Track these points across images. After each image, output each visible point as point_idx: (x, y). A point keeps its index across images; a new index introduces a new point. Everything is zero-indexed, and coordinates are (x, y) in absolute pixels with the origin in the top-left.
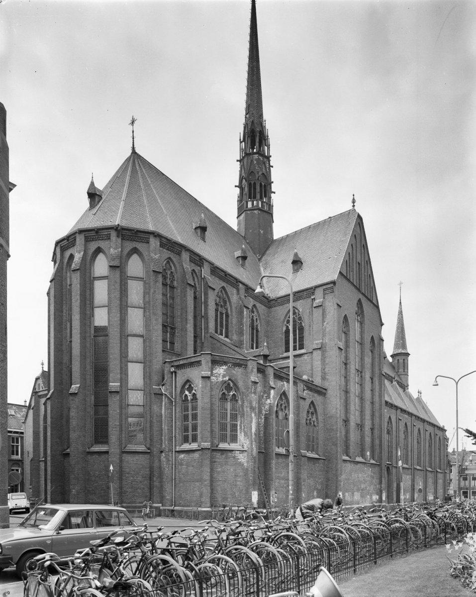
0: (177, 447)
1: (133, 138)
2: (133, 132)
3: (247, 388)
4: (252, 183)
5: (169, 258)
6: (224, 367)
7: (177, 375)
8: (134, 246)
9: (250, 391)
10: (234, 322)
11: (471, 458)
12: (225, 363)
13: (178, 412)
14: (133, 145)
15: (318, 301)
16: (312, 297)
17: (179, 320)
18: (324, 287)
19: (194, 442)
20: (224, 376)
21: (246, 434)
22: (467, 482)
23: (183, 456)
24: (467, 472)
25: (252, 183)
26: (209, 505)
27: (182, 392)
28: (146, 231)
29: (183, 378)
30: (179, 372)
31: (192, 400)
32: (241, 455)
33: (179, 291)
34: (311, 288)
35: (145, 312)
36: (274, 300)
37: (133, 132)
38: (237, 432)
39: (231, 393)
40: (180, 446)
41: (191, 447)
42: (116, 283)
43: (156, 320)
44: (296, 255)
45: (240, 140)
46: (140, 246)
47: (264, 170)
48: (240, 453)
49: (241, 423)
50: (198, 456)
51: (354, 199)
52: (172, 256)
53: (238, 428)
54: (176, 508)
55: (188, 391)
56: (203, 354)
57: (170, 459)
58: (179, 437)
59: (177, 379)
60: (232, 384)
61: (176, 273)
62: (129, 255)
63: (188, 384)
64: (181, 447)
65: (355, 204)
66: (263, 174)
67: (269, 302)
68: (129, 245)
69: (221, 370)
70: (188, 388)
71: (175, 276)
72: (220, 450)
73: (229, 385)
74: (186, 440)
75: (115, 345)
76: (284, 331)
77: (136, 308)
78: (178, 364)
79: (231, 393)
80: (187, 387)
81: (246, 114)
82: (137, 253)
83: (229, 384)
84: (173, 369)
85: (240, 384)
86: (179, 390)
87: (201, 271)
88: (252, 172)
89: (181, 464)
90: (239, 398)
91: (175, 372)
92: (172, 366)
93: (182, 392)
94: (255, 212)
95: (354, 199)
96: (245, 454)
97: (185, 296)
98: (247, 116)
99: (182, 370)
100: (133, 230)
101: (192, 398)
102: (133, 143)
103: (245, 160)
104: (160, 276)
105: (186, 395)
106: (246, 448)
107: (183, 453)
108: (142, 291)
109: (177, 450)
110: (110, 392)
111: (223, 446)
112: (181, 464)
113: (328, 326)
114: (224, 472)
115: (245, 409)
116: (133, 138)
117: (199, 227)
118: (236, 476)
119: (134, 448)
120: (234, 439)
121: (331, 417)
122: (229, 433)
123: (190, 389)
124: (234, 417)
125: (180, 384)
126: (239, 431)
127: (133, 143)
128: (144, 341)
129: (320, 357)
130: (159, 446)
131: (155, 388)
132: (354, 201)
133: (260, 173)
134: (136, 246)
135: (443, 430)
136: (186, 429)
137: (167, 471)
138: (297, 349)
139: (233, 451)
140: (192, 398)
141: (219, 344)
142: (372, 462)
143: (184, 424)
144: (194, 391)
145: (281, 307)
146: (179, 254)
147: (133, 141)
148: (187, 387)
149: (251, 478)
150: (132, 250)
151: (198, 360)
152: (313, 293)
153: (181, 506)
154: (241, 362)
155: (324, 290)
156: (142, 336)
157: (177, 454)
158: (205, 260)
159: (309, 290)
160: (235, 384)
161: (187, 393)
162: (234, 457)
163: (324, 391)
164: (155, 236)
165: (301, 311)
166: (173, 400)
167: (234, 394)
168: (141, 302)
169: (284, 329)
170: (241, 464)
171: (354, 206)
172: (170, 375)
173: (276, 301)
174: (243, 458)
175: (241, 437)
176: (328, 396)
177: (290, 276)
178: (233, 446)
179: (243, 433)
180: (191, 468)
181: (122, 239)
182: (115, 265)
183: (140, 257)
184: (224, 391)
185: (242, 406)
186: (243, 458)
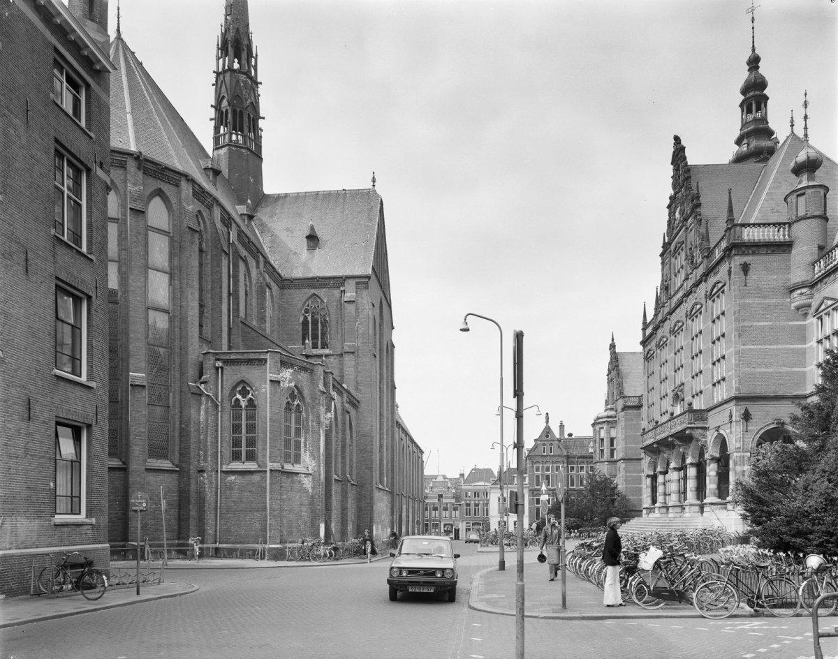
0: (224, 466)
1: (118, 18)
2: (118, 9)
3: (314, 398)
4: (238, 110)
5: (199, 212)
6: (291, 370)
7: (225, 372)
8: (159, 187)
9: (317, 402)
10: (254, 304)
11: (431, 485)
12: (292, 366)
13: (225, 420)
14: (119, 27)
15: (350, 295)
16: (341, 289)
17: (209, 295)
18: (358, 280)
19: (249, 460)
20: (290, 381)
21: (312, 455)
22: (427, 513)
23: (233, 478)
24: (427, 501)
25: (238, 110)
26: (278, 541)
27: (232, 394)
28: (171, 168)
29: (235, 377)
30: (228, 369)
31: (247, 406)
32: (306, 479)
33: (209, 257)
34: (341, 277)
35: (171, 279)
36: (289, 280)
37: (118, 9)
38: (300, 451)
39: (296, 403)
40: (228, 465)
41: (246, 467)
42: (140, 234)
43: (193, 294)
44: (312, 228)
45: (218, 45)
46: (168, 189)
47: (253, 98)
48: (305, 477)
49: (306, 440)
50: (259, 478)
51: (374, 178)
52: (202, 208)
53: (302, 445)
54: (221, 546)
55: (240, 394)
56: (270, 351)
57: (214, 481)
58: (227, 454)
59: (224, 378)
60: (296, 392)
61: (206, 233)
62: (152, 196)
63: (243, 387)
64: (230, 467)
65: (375, 184)
66: (252, 103)
67: (285, 284)
68: (154, 184)
69: (287, 374)
70: (240, 391)
71: (204, 237)
72: (286, 472)
73: (295, 393)
74: (236, 457)
75: (138, 320)
76: (301, 322)
77: (160, 271)
78: (228, 357)
79: (296, 403)
80: (239, 388)
81: (227, 15)
82: (160, 196)
83: (293, 391)
84: (219, 364)
85: (306, 392)
86: (227, 392)
87: (229, 233)
88: (238, 95)
89: (231, 489)
90: (303, 409)
91: (222, 368)
92: (218, 360)
93: (232, 394)
94: (244, 151)
95: (374, 178)
96: (310, 478)
97: (219, 265)
98: (228, 17)
99: (233, 367)
100: (160, 165)
101: (247, 404)
102: (119, 24)
103: (228, 76)
104: (197, 235)
105: (237, 400)
106: (310, 472)
107: (234, 475)
108: (168, 250)
109: (224, 470)
110: (132, 385)
111: (288, 467)
112: (231, 489)
113: (360, 326)
114: (289, 500)
115: (310, 423)
116: (118, 18)
117: (211, 168)
118: (301, 505)
119: (157, 465)
120: (297, 460)
121: (365, 436)
122: (244, 449)
123: (244, 393)
124: (298, 431)
125: (228, 386)
126: (302, 450)
127: (119, 24)
128: (170, 318)
129: (353, 363)
130: (196, 463)
131: (191, 385)
132: (374, 181)
133: (249, 102)
134: (162, 187)
135: (422, 452)
136: (237, 443)
137: (209, 497)
138: (320, 347)
139: (298, 473)
140: (247, 404)
141: (254, 334)
142: (387, 489)
143: (233, 437)
144: (250, 396)
145: (298, 291)
146: (210, 208)
147: (119, 21)
148: (239, 388)
149: (318, 507)
150: (155, 191)
151: (262, 357)
152: (343, 284)
153: (229, 543)
154: (308, 366)
155: (357, 283)
156: (167, 312)
157: (223, 475)
158: (233, 220)
159: (337, 279)
160: (300, 392)
161: (239, 396)
162: (299, 482)
163: (357, 403)
164: (188, 180)
165: (325, 301)
166: (219, 404)
167: (298, 405)
168: (167, 264)
169: (302, 319)
170: (305, 491)
171: (374, 186)
172: (214, 371)
173: (292, 282)
174: (307, 483)
175: (306, 457)
176: (361, 409)
177: (305, 254)
178: (297, 468)
179: (308, 453)
180: (246, 494)
181: (144, 173)
182: (138, 208)
183: (164, 202)
184: (289, 400)
185: (307, 419)
186: (307, 483)
